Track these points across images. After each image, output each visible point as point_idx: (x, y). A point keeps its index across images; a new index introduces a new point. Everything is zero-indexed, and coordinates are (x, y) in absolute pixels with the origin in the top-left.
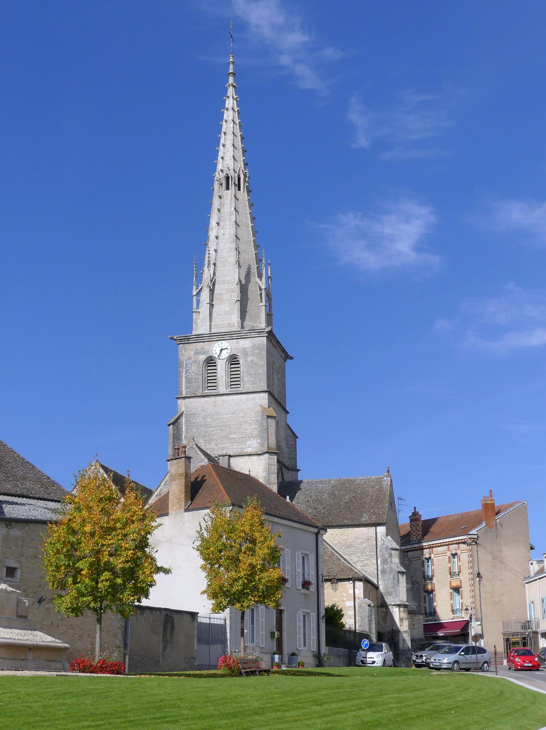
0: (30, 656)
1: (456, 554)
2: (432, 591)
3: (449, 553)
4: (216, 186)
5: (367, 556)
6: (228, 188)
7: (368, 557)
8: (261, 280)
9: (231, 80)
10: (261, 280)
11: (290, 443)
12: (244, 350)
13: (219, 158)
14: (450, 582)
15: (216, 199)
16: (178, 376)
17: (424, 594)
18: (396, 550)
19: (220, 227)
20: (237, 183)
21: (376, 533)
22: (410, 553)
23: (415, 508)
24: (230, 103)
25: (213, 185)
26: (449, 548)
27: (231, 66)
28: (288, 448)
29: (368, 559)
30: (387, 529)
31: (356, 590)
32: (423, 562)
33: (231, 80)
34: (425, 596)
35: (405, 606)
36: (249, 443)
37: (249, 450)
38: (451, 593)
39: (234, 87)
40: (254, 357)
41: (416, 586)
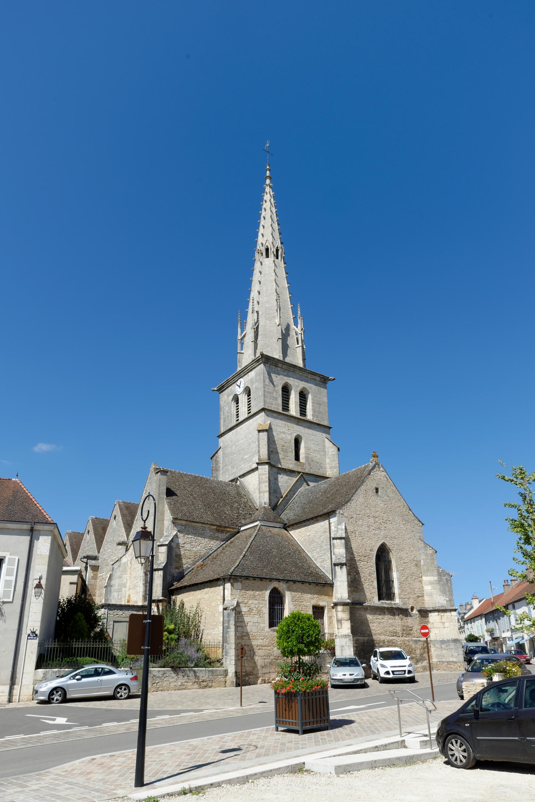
0: (292, 419)
4: (257, 256)
6: (267, 256)
8: (297, 327)
9: (268, 181)
10: (297, 327)
12: (252, 381)
13: (260, 235)
15: (257, 265)
19: (262, 275)
20: (275, 253)
24: (267, 197)
25: (254, 257)
31: (226, 591)
33: (268, 181)
39: (270, 187)
41: (444, 578)
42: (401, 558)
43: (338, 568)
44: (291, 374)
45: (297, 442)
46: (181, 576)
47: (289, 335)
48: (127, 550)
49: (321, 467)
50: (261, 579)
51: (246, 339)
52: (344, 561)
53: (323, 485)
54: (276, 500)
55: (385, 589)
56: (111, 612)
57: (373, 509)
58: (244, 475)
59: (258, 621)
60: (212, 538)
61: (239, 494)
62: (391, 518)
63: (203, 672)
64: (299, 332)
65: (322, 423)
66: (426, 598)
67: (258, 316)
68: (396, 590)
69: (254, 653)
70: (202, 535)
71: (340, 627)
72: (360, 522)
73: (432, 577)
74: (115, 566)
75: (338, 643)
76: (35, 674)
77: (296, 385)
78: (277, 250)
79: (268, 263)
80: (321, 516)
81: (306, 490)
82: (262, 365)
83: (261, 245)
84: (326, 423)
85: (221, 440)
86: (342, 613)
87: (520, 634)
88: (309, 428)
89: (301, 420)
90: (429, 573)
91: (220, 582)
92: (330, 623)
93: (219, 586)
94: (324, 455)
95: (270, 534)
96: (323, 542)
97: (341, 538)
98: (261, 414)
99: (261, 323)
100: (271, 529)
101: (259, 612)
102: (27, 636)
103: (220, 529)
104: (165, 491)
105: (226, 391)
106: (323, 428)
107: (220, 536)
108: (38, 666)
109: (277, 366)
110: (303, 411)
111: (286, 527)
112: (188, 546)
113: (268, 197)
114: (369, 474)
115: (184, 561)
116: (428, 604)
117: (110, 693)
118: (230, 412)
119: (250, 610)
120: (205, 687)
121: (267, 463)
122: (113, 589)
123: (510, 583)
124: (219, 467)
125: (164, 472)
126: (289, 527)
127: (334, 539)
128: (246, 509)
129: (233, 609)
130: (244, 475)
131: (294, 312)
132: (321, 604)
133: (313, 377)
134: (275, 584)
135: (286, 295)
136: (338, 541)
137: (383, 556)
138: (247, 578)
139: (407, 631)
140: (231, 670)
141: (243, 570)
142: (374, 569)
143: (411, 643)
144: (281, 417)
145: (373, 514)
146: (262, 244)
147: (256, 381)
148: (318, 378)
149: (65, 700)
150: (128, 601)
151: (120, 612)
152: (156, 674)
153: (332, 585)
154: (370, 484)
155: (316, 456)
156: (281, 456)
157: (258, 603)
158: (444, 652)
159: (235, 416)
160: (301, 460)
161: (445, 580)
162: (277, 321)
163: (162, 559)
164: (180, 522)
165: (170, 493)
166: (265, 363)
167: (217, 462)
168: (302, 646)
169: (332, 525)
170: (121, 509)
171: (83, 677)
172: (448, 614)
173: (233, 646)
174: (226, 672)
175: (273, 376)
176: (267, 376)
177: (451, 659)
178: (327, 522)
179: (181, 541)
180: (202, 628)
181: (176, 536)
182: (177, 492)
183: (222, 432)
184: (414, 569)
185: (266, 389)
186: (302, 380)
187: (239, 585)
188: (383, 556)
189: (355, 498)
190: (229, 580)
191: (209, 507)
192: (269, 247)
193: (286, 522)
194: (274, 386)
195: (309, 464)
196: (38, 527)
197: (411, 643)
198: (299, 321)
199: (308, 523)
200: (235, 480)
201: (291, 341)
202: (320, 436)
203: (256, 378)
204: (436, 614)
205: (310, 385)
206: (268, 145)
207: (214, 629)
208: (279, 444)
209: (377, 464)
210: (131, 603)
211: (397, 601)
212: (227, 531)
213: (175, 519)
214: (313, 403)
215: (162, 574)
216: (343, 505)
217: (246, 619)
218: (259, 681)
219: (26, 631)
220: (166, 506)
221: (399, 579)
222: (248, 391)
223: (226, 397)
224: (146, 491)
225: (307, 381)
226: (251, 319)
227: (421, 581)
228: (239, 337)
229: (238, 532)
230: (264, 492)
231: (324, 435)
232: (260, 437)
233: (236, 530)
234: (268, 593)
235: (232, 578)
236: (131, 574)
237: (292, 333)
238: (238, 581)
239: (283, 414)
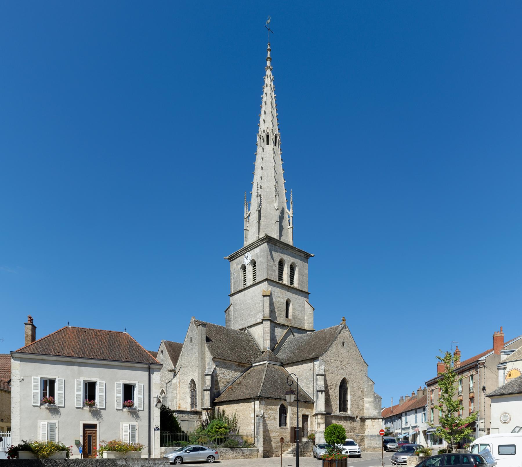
4: (259, 141)
6: (268, 143)
8: (289, 211)
9: (269, 63)
10: (289, 211)
13: (261, 120)
15: (259, 150)
16: (230, 282)
19: (264, 161)
20: (274, 140)
24: (268, 81)
25: (256, 142)
27: (269, 53)
31: (256, 406)
33: (269, 63)
39: (271, 70)
41: (377, 400)
42: (353, 387)
43: (319, 393)
44: (285, 251)
45: (287, 303)
46: (219, 394)
47: (283, 218)
48: (175, 375)
49: (302, 323)
50: (276, 399)
51: (251, 217)
52: (324, 389)
53: (306, 337)
54: (273, 345)
55: (343, 407)
56: (179, 415)
57: (340, 356)
58: (250, 327)
59: (273, 423)
60: (236, 370)
61: (248, 339)
62: (350, 362)
63: (246, 450)
64: (291, 215)
65: (303, 290)
66: (365, 411)
67: (261, 199)
68: (349, 406)
69: (271, 441)
70: (230, 369)
72: (332, 365)
74: (168, 385)
75: (317, 436)
76: (161, 450)
77: (289, 260)
78: (276, 137)
79: (268, 150)
80: (308, 360)
81: (293, 339)
82: (266, 244)
83: (263, 132)
84: (306, 290)
85: (231, 298)
86: (321, 420)
87: (407, 431)
88: (296, 294)
89: (290, 288)
91: (251, 400)
92: (311, 424)
93: (251, 402)
94: (304, 313)
95: (274, 369)
96: (308, 376)
97: (322, 375)
98: (264, 283)
99: (263, 206)
100: (274, 366)
101: (274, 418)
103: (241, 365)
104: (205, 338)
105: (236, 261)
106: (304, 294)
108: (161, 445)
109: (276, 245)
110: (292, 282)
111: (283, 365)
112: (222, 375)
114: (340, 333)
115: (220, 385)
116: (366, 414)
117: (205, 460)
118: (238, 277)
119: (269, 417)
120: (247, 458)
121: (269, 320)
122: (168, 399)
123: (404, 398)
124: (231, 319)
125: (204, 325)
126: (285, 365)
127: (317, 375)
128: (255, 352)
129: (261, 416)
130: (250, 327)
131: (288, 198)
132: (307, 413)
133: (300, 254)
135: (282, 182)
137: (343, 385)
138: (268, 398)
139: (353, 430)
140: (261, 449)
141: (265, 393)
142: (338, 393)
143: (354, 436)
144: (278, 285)
145: (340, 359)
146: (264, 130)
148: (303, 255)
149: (183, 463)
150: (179, 408)
151: (184, 415)
152: (222, 450)
153: (313, 403)
154: (339, 340)
155: (299, 315)
156: (277, 314)
157: (274, 411)
158: (372, 442)
159: (243, 281)
160: (289, 318)
161: (377, 400)
162: (276, 205)
164: (217, 360)
165: (208, 340)
166: (268, 243)
167: (229, 315)
168: (338, 440)
169: (316, 366)
170: (166, 347)
171: (191, 451)
172: (377, 420)
173: (262, 437)
174: (258, 451)
175: (273, 252)
176: (269, 253)
177: (376, 446)
178: (312, 364)
179: (218, 372)
180: (238, 425)
181: (215, 368)
182: (211, 339)
184: (360, 394)
185: (268, 264)
186: (292, 257)
187: (263, 402)
188: (343, 385)
189: (330, 349)
190: (258, 399)
191: (230, 349)
192: (270, 134)
193: (283, 361)
194: (274, 261)
195: (295, 320)
196: (152, 366)
197: (354, 436)
198: (291, 206)
199: (298, 363)
200: (244, 329)
201: (285, 223)
202: (302, 299)
203: (260, 253)
204: (370, 420)
205: (297, 260)
206: (269, 21)
207: (247, 427)
208: (276, 305)
209: (345, 326)
210: (181, 409)
211: (349, 413)
212: (244, 366)
213: (214, 358)
214: (299, 274)
216: (323, 354)
217: (267, 422)
218: (274, 455)
219: (153, 426)
220: (207, 349)
221: (351, 399)
222: (254, 263)
223: (235, 266)
224: (188, 336)
225: (295, 257)
226: (254, 202)
227: (363, 401)
229: (252, 367)
230: (267, 340)
231: (305, 299)
232: (265, 301)
233: (250, 366)
234: (279, 407)
235: (260, 398)
236: (180, 391)
237: (286, 216)
239: (278, 283)
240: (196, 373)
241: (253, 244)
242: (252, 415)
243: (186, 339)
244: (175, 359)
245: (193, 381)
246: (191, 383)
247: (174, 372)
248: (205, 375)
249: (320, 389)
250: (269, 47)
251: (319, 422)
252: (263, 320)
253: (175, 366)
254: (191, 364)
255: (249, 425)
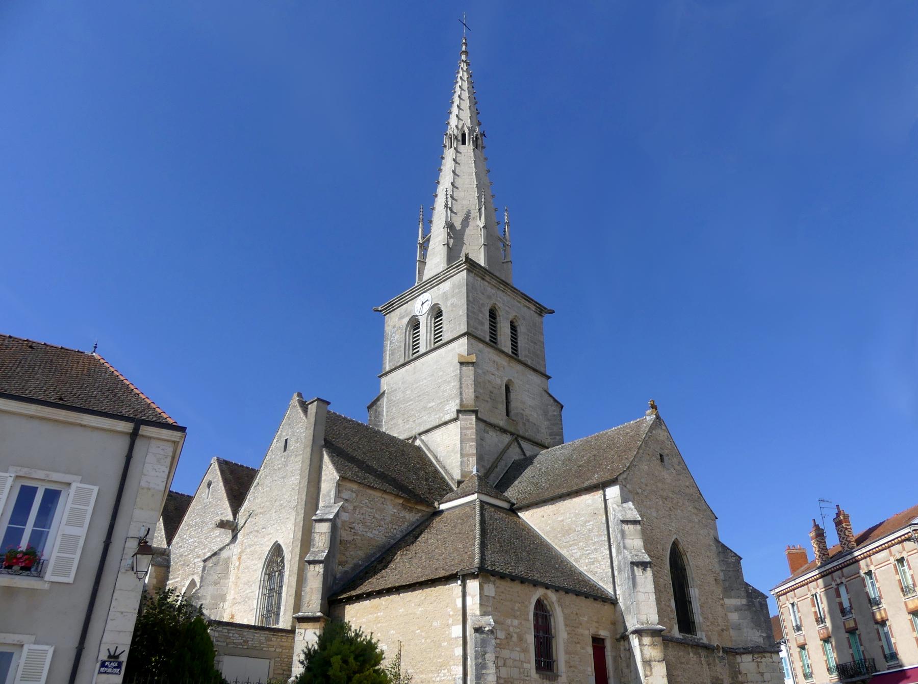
1: (903, 558)
2: (883, 623)
3: (892, 560)
5: (594, 543)
6: (464, 143)
7: (597, 546)
11: (550, 413)
12: (445, 296)
14: (905, 603)
17: (876, 626)
18: (635, 522)
21: (605, 500)
22: (845, 570)
23: (838, 506)
26: (890, 552)
28: (549, 420)
29: (596, 550)
30: (621, 490)
31: (469, 599)
32: (863, 580)
34: (878, 630)
35: (654, 633)
36: (447, 407)
37: (447, 418)
38: (911, 620)
40: (454, 299)
43: (638, 571)
50: (523, 581)
71: (649, 673)
73: (739, 600)
74: (210, 564)
90: (733, 593)
96: (590, 531)
102: (98, 665)
107: (407, 517)
109: (483, 279)
113: (463, 74)
134: (539, 592)
136: (631, 527)
147: (453, 296)
148: (533, 308)
150: (232, 617)
163: (321, 544)
183: (387, 369)
207: (438, 671)
215: (322, 570)
219: (97, 651)
224: (280, 437)
228: (420, 240)
230: (469, 455)
238: (489, 581)
240: (290, 525)
241: (437, 276)
242: (457, 631)
243: (274, 445)
244: (237, 497)
245: (277, 550)
246: (273, 555)
247: (231, 527)
248: (316, 521)
249: (636, 559)
250: (464, 48)
251: (647, 656)
252: (458, 412)
253: (235, 513)
254: (278, 503)
255: (443, 666)
